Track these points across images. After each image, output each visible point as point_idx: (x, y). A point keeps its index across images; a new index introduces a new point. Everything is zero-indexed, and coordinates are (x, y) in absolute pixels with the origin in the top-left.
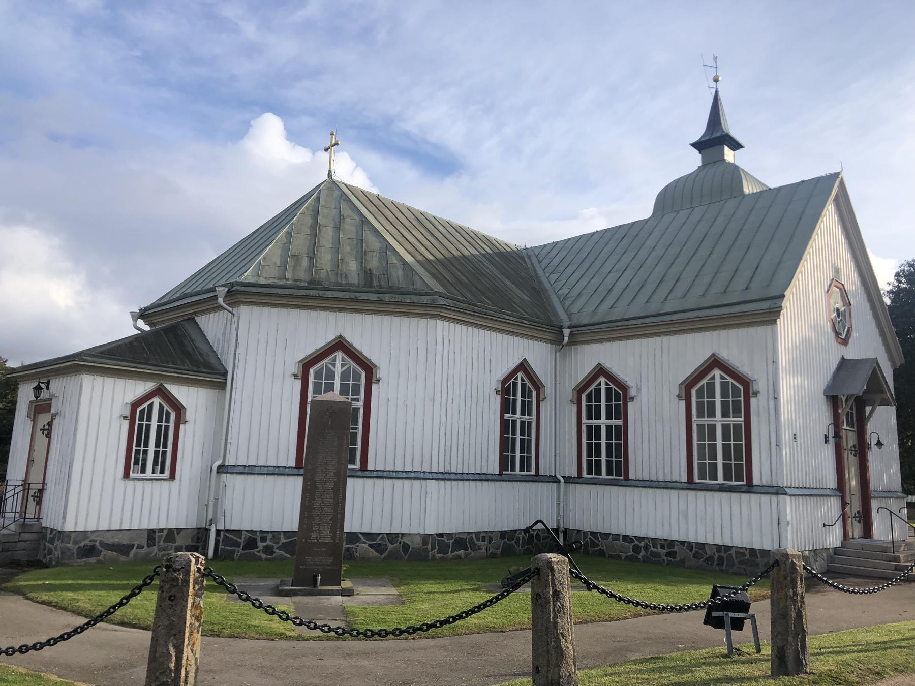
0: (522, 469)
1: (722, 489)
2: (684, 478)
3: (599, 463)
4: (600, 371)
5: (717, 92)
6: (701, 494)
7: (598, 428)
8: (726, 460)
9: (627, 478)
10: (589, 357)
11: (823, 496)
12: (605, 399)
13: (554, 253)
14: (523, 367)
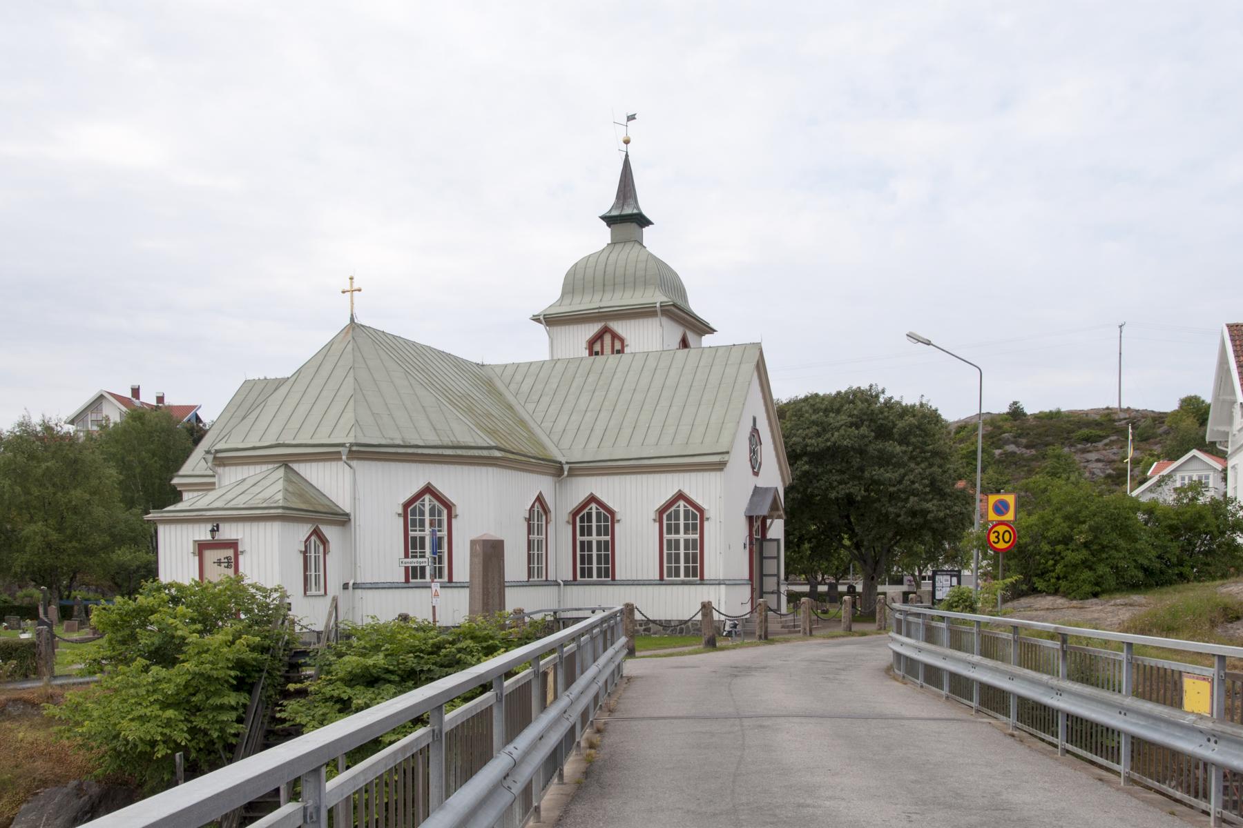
1: (683, 583)
4: (592, 499)
5: (627, 156)
8: (682, 563)
10: (582, 488)
12: (595, 521)
13: (518, 378)
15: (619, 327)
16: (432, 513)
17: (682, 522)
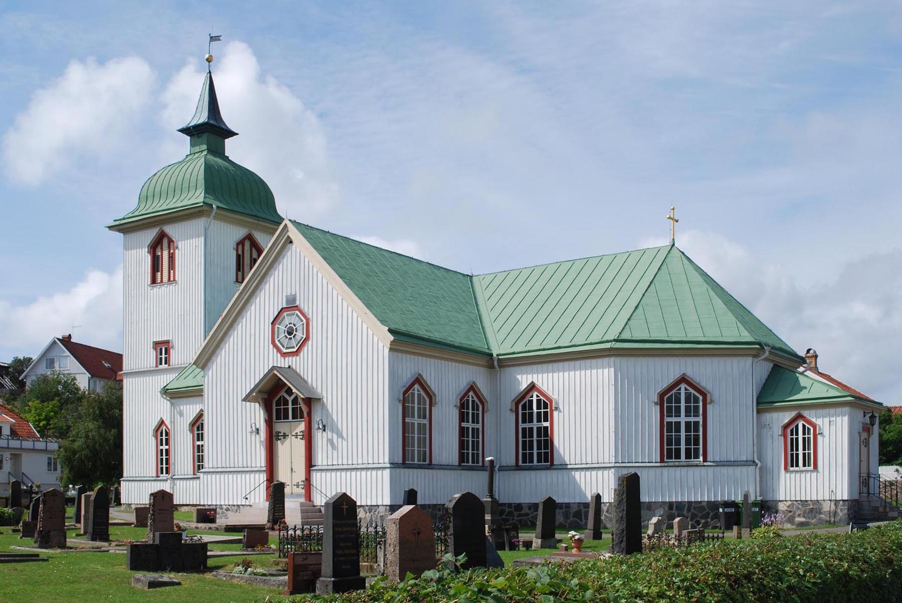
0: (473, 462)
3: (531, 455)
7: (531, 429)
9: (552, 464)
11: (247, 471)
14: (472, 388)
15: (170, 230)
16: (688, 400)
17: (683, 405)
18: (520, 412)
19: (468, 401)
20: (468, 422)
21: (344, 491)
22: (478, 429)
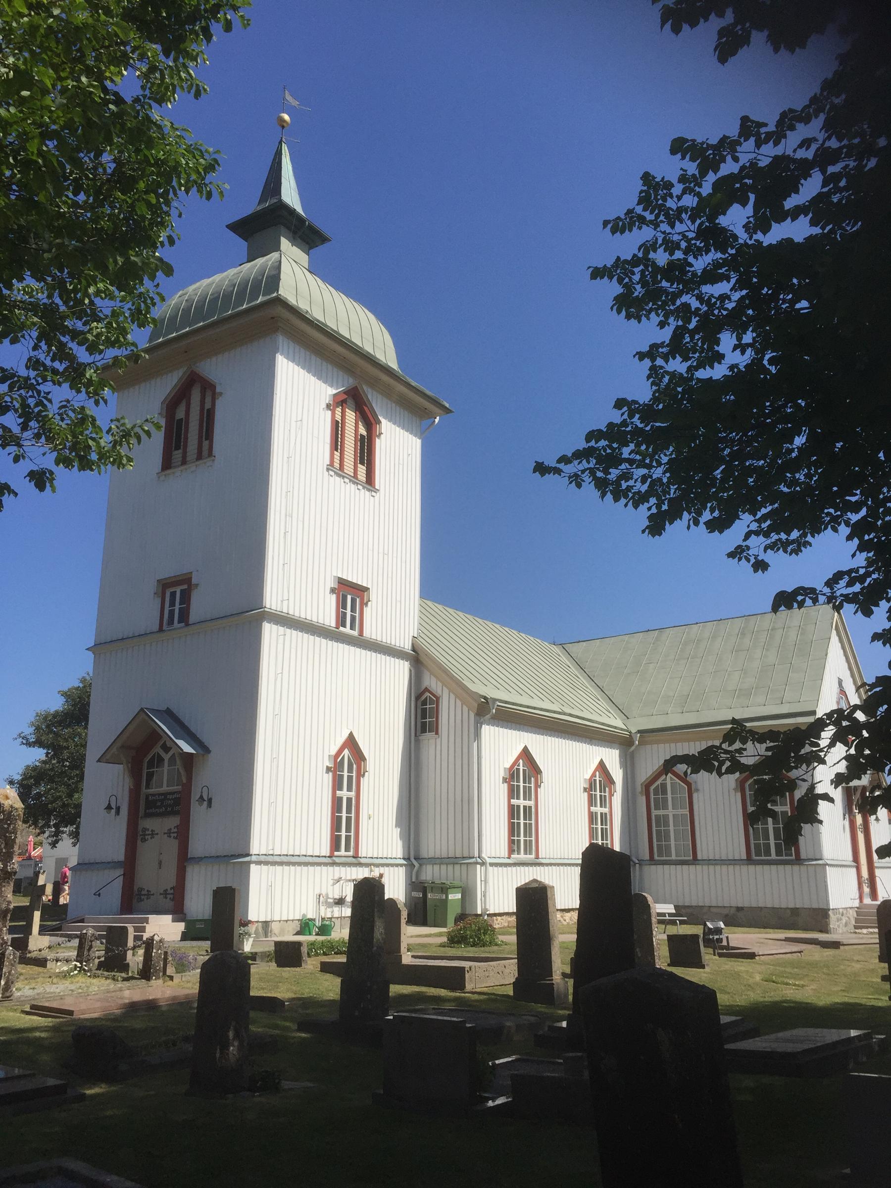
2: (744, 857)
6: (660, 867)
18: (652, 796)
19: (518, 770)
20: (518, 798)
21: (304, 911)
22: (530, 807)
